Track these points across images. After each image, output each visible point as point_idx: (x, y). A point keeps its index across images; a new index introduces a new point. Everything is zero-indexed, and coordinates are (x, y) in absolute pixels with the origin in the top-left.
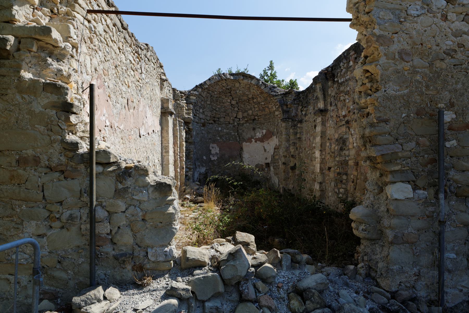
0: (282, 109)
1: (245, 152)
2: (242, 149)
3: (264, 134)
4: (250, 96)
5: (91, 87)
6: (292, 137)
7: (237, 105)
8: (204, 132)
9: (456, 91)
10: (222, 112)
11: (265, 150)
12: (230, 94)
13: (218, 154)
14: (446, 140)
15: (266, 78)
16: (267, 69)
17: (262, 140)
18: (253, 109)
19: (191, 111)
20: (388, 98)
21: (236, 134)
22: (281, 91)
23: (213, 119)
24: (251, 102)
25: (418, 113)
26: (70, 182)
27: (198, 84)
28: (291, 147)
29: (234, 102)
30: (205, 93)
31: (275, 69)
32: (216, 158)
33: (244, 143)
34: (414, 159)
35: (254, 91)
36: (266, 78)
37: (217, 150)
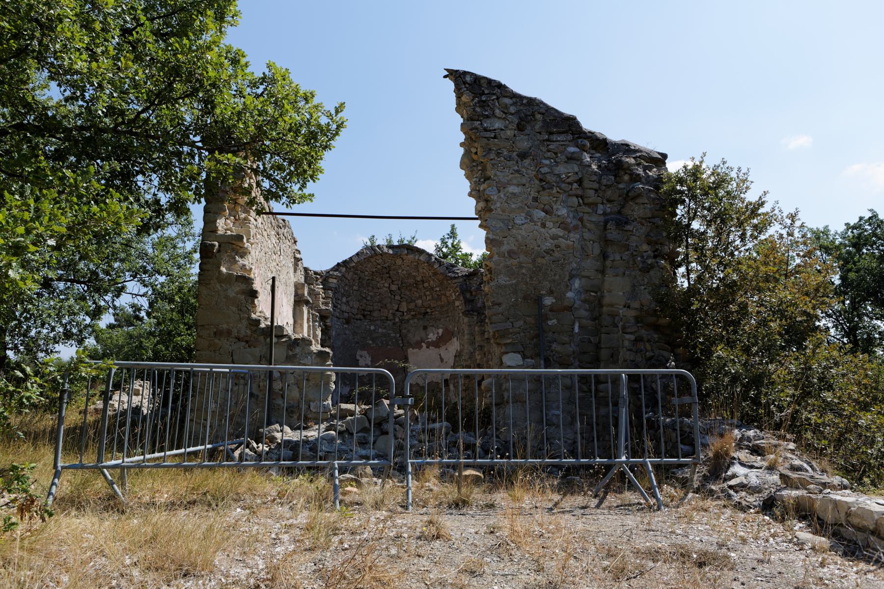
0: (464, 298)
4: (419, 279)
5: (274, 278)
6: (478, 338)
8: (347, 332)
9: (554, 281)
14: (547, 319)
15: (445, 250)
16: (446, 236)
17: (437, 344)
19: (330, 300)
20: (499, 287)
22: (461, 270)
24: (421, 286)
25: (525, 298)
26: (253, 349)
27: (340, 261)
28: (477, 353)
29: (394, 287)
30: (351, 273)
31: (458, 238)
33: (410, 350)
34: (522, 334)
36: (445, 250)
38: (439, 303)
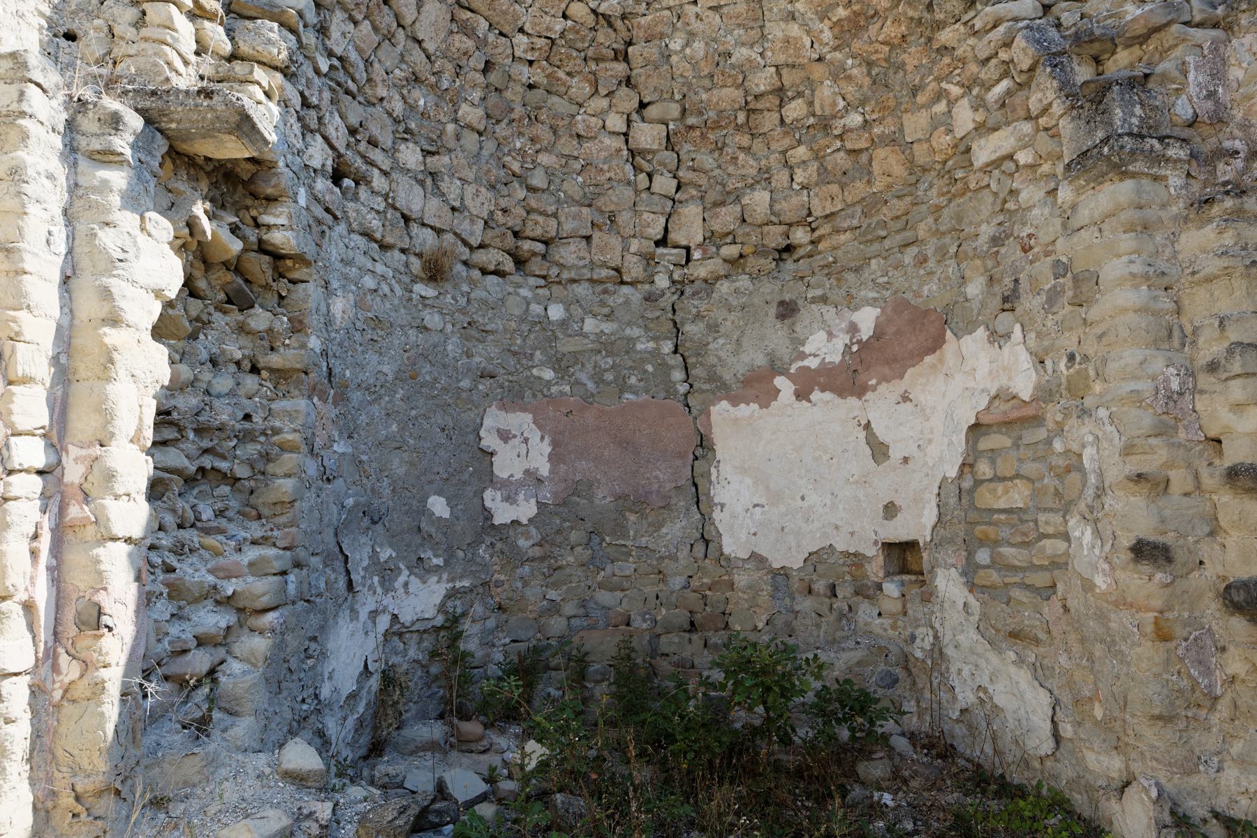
1: (726, 469)
2: (704, 444)
3: (866, 332)
7: (670, 157)
8: (433, 320)
10: (571, 200)
11: (879, 451)
12: (620, 68)
13: (540, 481)
17: (848, 379)
18: (781, 177)
21: (667, 347)
23: (510, 241)
24: (769, 121)
29: (647, 135)
32: (525, 510)
33: (721, 411)
35: (794, 30)
37: (539, 458)
38: (860, 188)
